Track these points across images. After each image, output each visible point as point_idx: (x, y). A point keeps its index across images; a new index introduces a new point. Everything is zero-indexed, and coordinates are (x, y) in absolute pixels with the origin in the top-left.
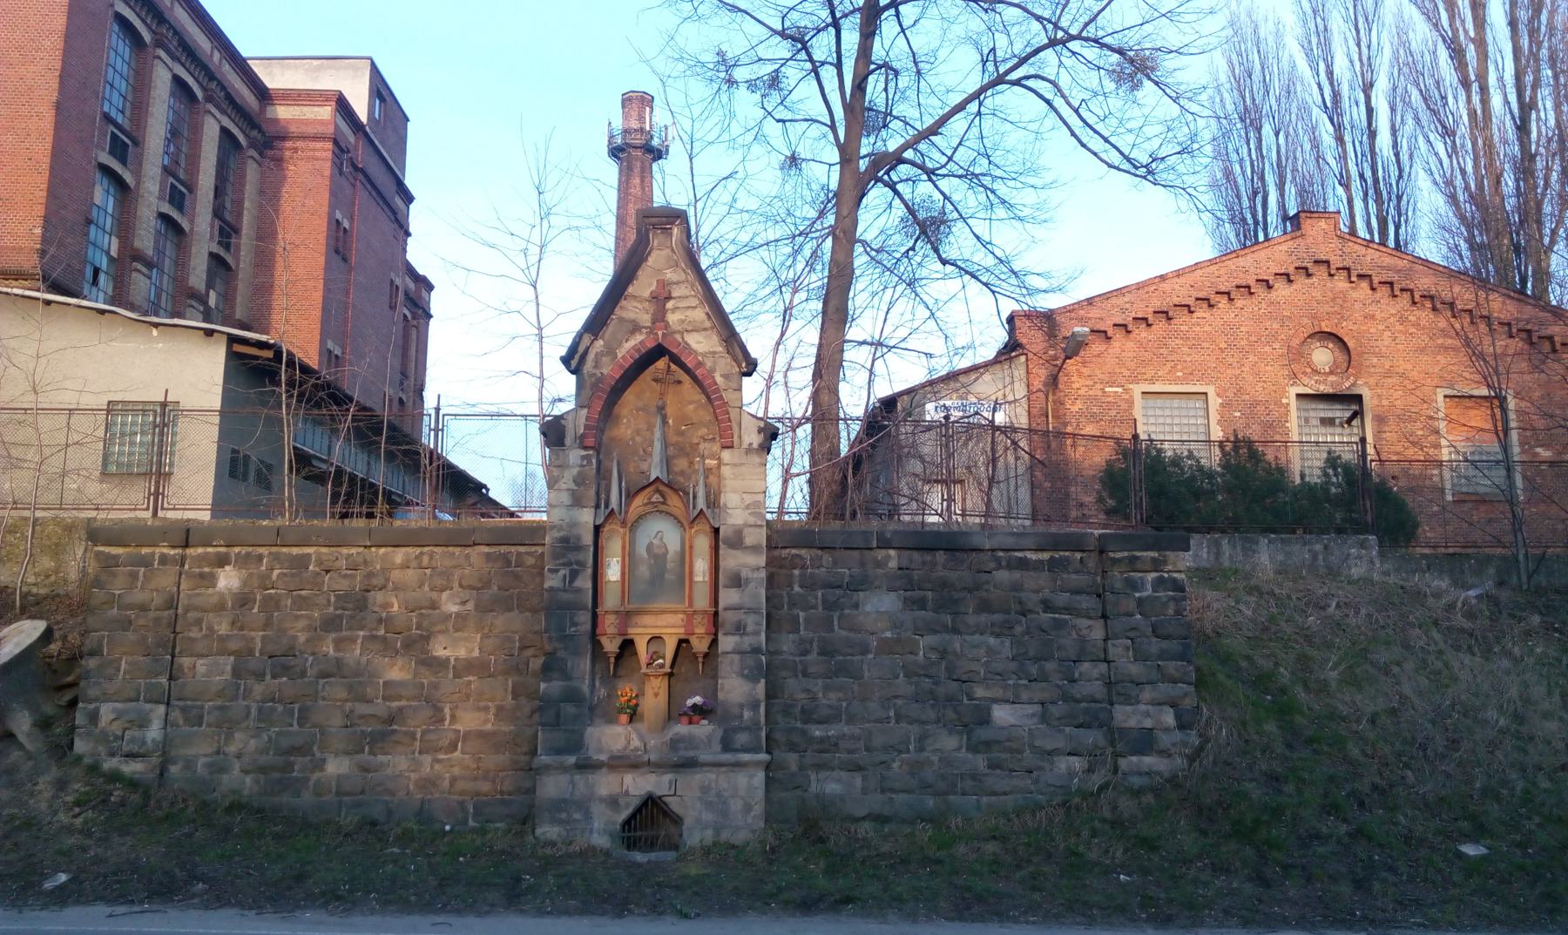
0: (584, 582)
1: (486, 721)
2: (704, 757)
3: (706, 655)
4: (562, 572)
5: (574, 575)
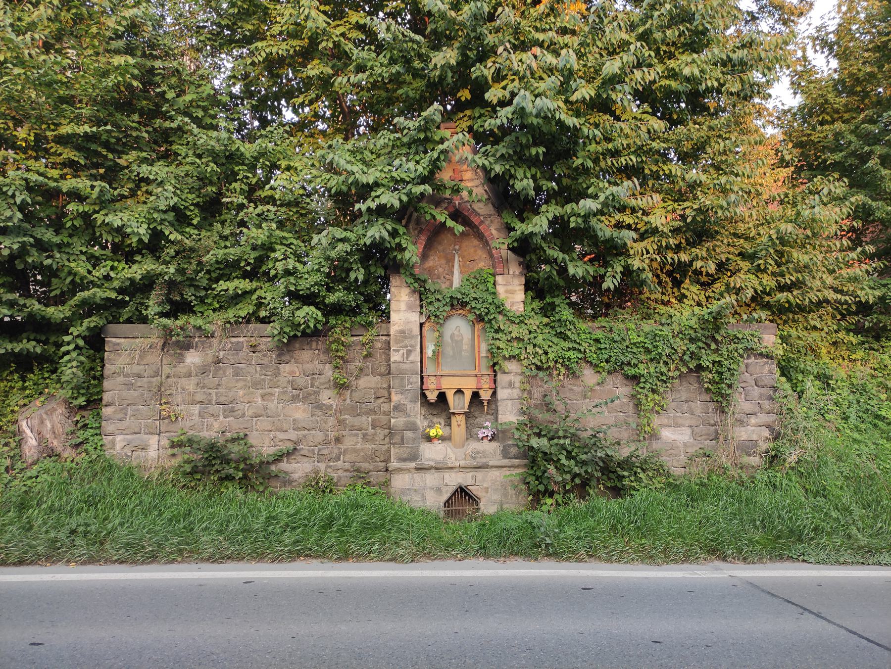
0: (415, 357)
2: (491, 463)
3: (489, 402)
5: (409, 353)
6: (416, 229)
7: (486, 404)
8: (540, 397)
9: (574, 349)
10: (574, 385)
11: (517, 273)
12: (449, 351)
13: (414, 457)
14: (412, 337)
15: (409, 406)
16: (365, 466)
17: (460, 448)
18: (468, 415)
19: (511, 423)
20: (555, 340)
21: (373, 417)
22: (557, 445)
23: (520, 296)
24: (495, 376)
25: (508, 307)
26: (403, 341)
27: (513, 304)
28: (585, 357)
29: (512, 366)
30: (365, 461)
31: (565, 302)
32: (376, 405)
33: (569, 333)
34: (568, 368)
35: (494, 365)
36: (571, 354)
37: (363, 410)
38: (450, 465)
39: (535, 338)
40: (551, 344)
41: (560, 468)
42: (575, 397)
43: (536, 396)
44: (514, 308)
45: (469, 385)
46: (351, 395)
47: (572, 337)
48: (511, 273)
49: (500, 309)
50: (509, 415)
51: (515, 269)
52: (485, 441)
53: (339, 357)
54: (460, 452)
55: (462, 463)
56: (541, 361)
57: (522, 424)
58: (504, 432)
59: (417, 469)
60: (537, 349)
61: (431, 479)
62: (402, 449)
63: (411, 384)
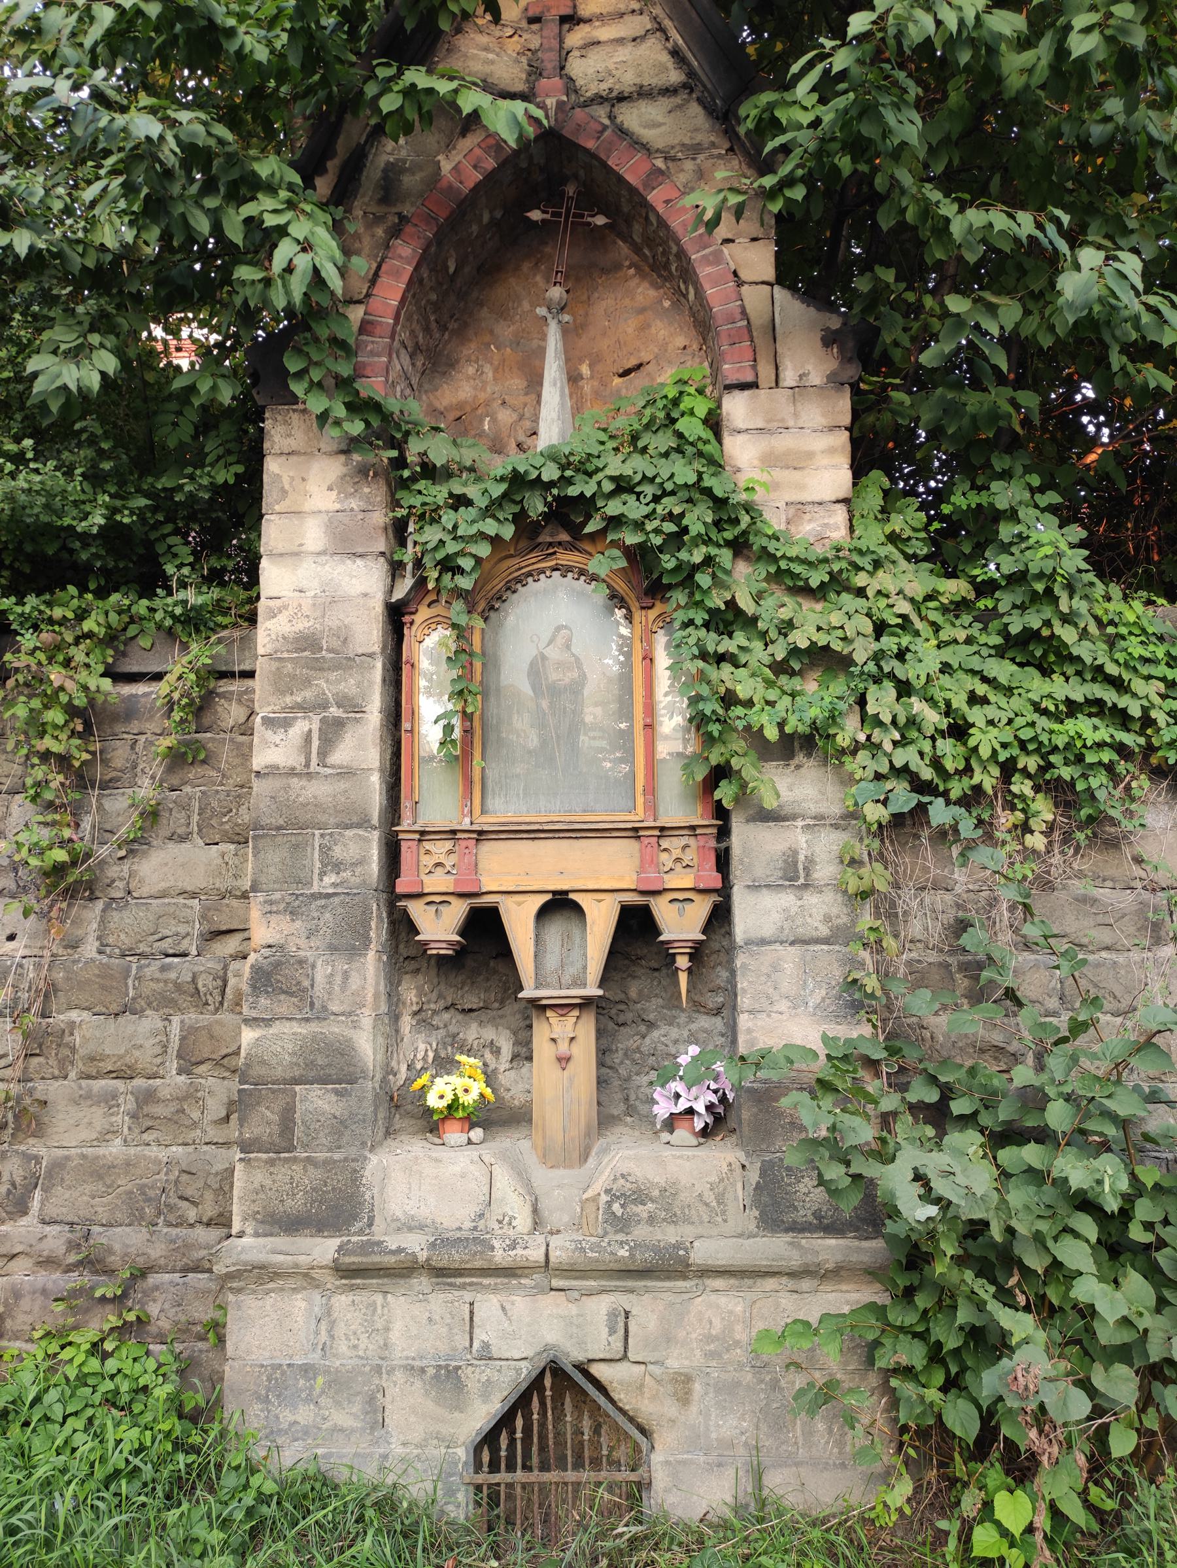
0: (363, 747)
1: (105, 1136)
2: (703, 1252)
3: (697, 953)
4: (300, 727)
5: (332, 731)
6: (378, 219)
7: (683, 962)
8: (936, 933)
9: (1097, 707)
10: (1100, 879)
11: (816, 378)
12: (521, 728)
13: (338, 1208)
14: (347, 663)
15: (321, 972)
16: (127, 1241)
17: (567, 1164)
18: (606, 1011)
19: (793, 1054)
20: (1002, 670)
21: (192, 1017)
22: (1036, 1176)
23: (831, 475)
24: (724, 832)
25: (775, 521)
26: (307, 683)
27: (800, 508)
28: (1150, 749)
29: (798, 786)
30: (136, 1218)
31: (1044, 500)
32: (208, 963)
33: (1068, 634)
34: (1064, 795)
35: (720, 773)
36: (1086, 728)
37: (149, 988)
38: (500, 1256)
39: (901, 655)
40: (982, 689)
41: (1077, 1334)
42: (1105, 936)
43: (916, 928)
44: (807, 529)
45: (604, 873)
46: (103, 922)
47: (1083, 650)
48: (789, 377)
49: (736, 527)
50: (788, 1011)
51: (806, 361)
52: (682, 1135)
53: (46, 756)
54: (562, 1189)
55: (562, 1249)
56: (936, 763)
57: (846, 1058)
58: (765, 1096)
59: (351, 1273)
60: (918, 706)
61: (413, 1322)
62: (283, 1173)
63: (338, 867)
